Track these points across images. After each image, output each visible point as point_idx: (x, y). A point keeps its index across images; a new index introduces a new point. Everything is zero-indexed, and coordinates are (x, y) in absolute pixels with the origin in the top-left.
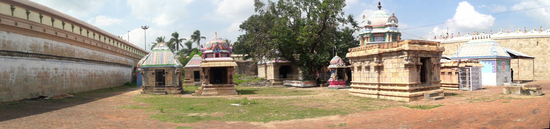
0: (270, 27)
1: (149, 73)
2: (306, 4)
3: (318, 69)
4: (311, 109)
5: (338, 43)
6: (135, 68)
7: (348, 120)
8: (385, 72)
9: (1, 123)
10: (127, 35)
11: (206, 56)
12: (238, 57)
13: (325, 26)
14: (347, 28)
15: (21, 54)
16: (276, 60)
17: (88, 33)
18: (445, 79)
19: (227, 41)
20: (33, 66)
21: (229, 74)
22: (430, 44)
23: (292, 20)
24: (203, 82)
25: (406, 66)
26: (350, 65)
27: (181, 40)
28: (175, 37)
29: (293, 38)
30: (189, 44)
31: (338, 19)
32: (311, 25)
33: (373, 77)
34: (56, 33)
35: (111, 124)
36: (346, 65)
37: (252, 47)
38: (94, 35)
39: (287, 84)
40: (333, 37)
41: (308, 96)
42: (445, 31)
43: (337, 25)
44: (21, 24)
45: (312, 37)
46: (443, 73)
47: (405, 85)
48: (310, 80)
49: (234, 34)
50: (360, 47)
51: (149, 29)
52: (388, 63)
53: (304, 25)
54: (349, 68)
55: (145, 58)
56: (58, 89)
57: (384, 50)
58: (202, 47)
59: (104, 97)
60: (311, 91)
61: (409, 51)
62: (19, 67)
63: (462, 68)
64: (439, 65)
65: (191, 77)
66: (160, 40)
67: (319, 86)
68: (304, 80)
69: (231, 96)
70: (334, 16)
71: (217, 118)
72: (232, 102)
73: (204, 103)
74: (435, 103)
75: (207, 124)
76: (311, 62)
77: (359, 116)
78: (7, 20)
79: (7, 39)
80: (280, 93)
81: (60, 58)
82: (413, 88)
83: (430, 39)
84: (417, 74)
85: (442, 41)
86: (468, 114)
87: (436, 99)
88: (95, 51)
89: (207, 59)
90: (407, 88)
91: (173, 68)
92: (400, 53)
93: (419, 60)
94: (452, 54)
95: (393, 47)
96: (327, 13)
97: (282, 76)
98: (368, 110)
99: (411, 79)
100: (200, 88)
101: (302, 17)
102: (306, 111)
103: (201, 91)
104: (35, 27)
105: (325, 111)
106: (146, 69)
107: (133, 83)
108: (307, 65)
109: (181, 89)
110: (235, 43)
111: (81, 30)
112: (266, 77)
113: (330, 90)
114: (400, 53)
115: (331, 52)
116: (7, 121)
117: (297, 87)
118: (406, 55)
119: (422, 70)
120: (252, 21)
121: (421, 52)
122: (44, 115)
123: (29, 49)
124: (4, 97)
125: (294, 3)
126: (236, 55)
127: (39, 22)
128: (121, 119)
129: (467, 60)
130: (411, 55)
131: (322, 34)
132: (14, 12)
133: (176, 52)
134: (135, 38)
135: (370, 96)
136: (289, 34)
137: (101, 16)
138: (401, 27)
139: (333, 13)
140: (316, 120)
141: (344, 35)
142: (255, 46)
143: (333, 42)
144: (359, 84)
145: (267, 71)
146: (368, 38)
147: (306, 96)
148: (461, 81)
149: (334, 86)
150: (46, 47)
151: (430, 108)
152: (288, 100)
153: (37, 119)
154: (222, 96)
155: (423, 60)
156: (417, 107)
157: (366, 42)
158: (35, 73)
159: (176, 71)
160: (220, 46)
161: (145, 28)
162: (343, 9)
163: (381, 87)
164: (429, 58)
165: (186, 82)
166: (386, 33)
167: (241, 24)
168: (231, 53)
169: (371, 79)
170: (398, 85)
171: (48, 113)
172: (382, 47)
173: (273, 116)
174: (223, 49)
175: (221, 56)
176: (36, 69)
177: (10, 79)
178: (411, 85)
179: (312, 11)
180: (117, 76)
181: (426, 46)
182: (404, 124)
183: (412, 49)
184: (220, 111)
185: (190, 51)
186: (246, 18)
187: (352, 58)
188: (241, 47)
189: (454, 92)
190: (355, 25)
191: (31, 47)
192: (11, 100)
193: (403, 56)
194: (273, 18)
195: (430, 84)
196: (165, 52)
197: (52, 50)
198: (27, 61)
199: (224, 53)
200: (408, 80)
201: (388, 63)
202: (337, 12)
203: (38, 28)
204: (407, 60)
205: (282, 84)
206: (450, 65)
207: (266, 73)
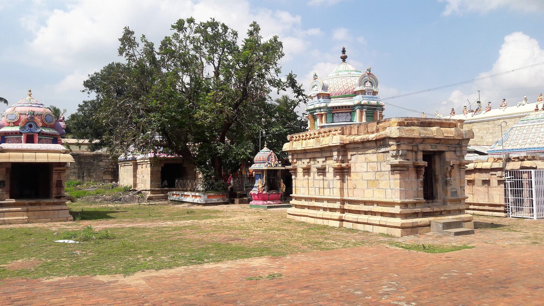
0: (145, 90)
2: (213, 51)
3: (231, 172)
4: (218, 246)
5: (269, 125)
7: (286, 266)
8: (353, 179)
13: (245, 94)
14: (286, 98)
16: (155, 152)
18: (474, 195)
21: (55, 177)
22: (441, 124)
23: (186, 79)
25: (394, 168)
26: (290, 164)
29: (188, 114)
31: (270, 81)
32: (222, 90)
33: (331, 187)
36: (283, 165)
39: (175, 197)
40: (261, 114)
41: (213, 221)
42: (474, 98)
43: (268, 92)
45: (221, 112)
46: (471, 182)
47: (392, 204)
48: (217, 190)
49: (71, 97)
50: (308, 133)
52: (359, 162)
53: (208, 91)
54: (288, 170)
57: (351, 138)
60: (218, 211)
61: (399, 140)
63: (513, 173)
64: (461, 166)
67: (233, 202)
68: (206, 191)
69: (58, 224)
70: (262, 76)
72: (59, 236)
74: (451, 239)
76: (220, 158)
77: (305, 259)
80: (160, 216)
82: (409, 210)
83: (443, 115)
84: (416, 184)
85: (469, 117)
86: (529, 269)
87: (457, 234)
90: (397, 210)
92: (381, 142)
93: (420, 156)
94: (486, 145)
95: (368, 133)
96: (250, 69)
97: (166, 182)
98: (322, 249)
99: (404, 192)
101: (205, 75)
102: (208, 248)
105: (242, 249)
108: (213, 163)
110: (73, 117)
112: (135, 185)
113: (254, 210)
114: (381, 142)
115: (255, 141)
117: (193, 204)
118: (394, 147)
119: (426, 175)
120: (110, 73)
121: (424, 140)
125: (191, 46)
126: (74, 141)
129: (523, 155)
130: (404, 147)
131: (241, 108)
135: (326, 222)
136: (181, 105)
138: (385, 94)
139: (260, 69)
140: (224, 266)
141: (279, 109)
142: (115, 124)
143: (260, 124)
144: (306, 199)
145: (137, 174)
146: (322, 115)
147: (208, 221)
148: (511, 198)
149: (261, 203)
151: (443, 250)
152: (175, 229)
154: (36, 225)
155: (428, 156)
156: (417, 248)
157: (318, 123)
160: (38, 120)
162: (279, 62)
163: (347, 206)
164: (441, 153)
166: (355, 106)
167: (87, 78)
169: (327, 191)
170: (379, 203)
172: (347, 132)
173: (142, 260)
174: (45, 126)
178: (404, 205)
179: (224, 65)
181: (434, 129)
182: (391, 279)
183: (404, 135)
184: (30, 256)
186: (98, 68)
187: (294, 153)
188: (84, 125)
189: (496, 221)
190: (299, 92)
193: (388, 149)
194: (151, 73)
195: (444, 203)
199: (47, 135)
200: (398, 194)
201: (359, 162)
202: (267, 69)
204: (395, 157)
205: (166, 198)
206: (487, 165)
207: (135, 176)
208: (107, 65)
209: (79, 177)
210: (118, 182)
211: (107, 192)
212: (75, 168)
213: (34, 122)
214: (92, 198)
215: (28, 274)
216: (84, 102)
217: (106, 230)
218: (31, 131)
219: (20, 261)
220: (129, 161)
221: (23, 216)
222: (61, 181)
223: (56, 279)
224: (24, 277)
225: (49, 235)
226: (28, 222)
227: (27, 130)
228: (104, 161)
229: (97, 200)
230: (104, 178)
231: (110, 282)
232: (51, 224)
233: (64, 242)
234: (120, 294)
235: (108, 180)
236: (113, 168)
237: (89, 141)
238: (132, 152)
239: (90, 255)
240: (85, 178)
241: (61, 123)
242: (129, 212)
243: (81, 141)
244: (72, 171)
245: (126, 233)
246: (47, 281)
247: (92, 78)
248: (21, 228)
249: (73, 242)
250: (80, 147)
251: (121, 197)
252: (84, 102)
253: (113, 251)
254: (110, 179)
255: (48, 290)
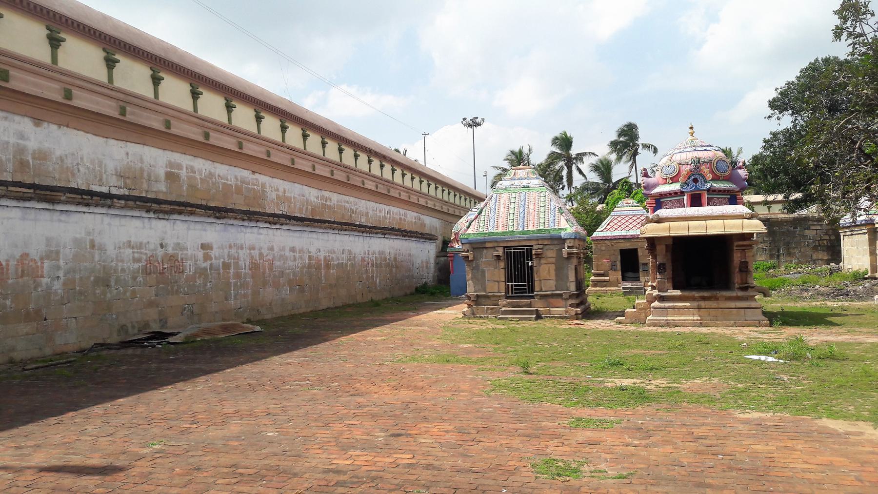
1: (487, 257)
6: (446, 243)
9: (5, 434)
10: (420, 145)
11: (659, 201)
12: (767, 203)
15: (105, 200)
17: (305, 137)
19: (727, 152)
20: (127, 236)
21: (737, 257)
24: (650, 284)
27: (580, 157)
28: (561, 147)
30: (603, 169)
34: (207, 136)
35: (375, 410)
37: (817, 166)
38: (324, 144)
44: (85, 95)
49: (749, 128)
51: (484, 125)
55: (475, 211)
56: (213, 307)
58: (646, 175)
59: (354, 329)
62: (77, 242)
65: (613, 267)
66: (518, 159)
69: (746, 330)
71: (701, 398)
72: (750, 349)
73: (654, 348)
75: (671, 416)
78: (31, 78)
79: (32, 145)
81: (220, 213)
88: (327, 194)
89: (662, 213)
91: (558, 241)
100: (641, 301)
103: (646, 310)
104: (137, 111)
106: (479, 246)
107: (440, 287)
109: (583, 302)
110: (756, 159)
111: (284, 129)
116: (30, 427)
122: (166, 392)
123: (113, 181)
124: (22, 341)
127: (150, 95)
128: (405, 394)
132: (60, 52)
133: (566, 192)
134: (446, 154)
137: (344, 87)
150: (172, 177)
153: (142, 409)
154: (713, 330)
158: (135, 260)
159: (565, 250)
160: (706, 170)
161: (474, 124)
165: (596, 284)
167: (774, 95)
168: (743, 190)
171: (180, 385)
174: (716, 179)
175: (711, 203)
176: (140, 246)
177: (45, 280)
180: (393, 265)
184: (711, 376)
185: (606, 188)
188: (777, 170)
191: (120, 176)
192: (48, 351)
196: (533, 196)
197: (192, 187)
198: (107, 220)
203: (146, 114)
208: (806, 65)
209: (772, 257)
210: (841, 264)
211: (823, 281)
212: (764, 242)
213: (700, 175)
214: (796, 291)
215: (712, 401)
216: (771, 133)
217: (830, 344)
218: (697, 189)
219: (698, 381)
220: (861, 225)
221: (693, 315)
222: (747, 263)
223: (755, 415)
224: (707, 405)
225: (732, 345)
226: (701, 325)
227: (691, 187)
228: (812, 227)
229: (805, 294)
230: (814, 257)
231: (847, 433)
232: (735, 330)
233: (759, 360)
234: (871, 456)
235: (822, 260)
236: (830, 240)
237: (784, 197)
238: (865, 210)
239: (806, 384)
240: (783, 258)
241: (741, 172)
242: (868, 316)
243: (771, 198)
244: (760, 246)
245: (866, 351)
246: (741, 416)
247: (781, 93)
248: (692, 333)
249: (774, 360)
250: (769, 208)
251: (848, 289)
252: (771, 133)
253: (847, 382)
254: (826, 258)
255: (745, 429)
